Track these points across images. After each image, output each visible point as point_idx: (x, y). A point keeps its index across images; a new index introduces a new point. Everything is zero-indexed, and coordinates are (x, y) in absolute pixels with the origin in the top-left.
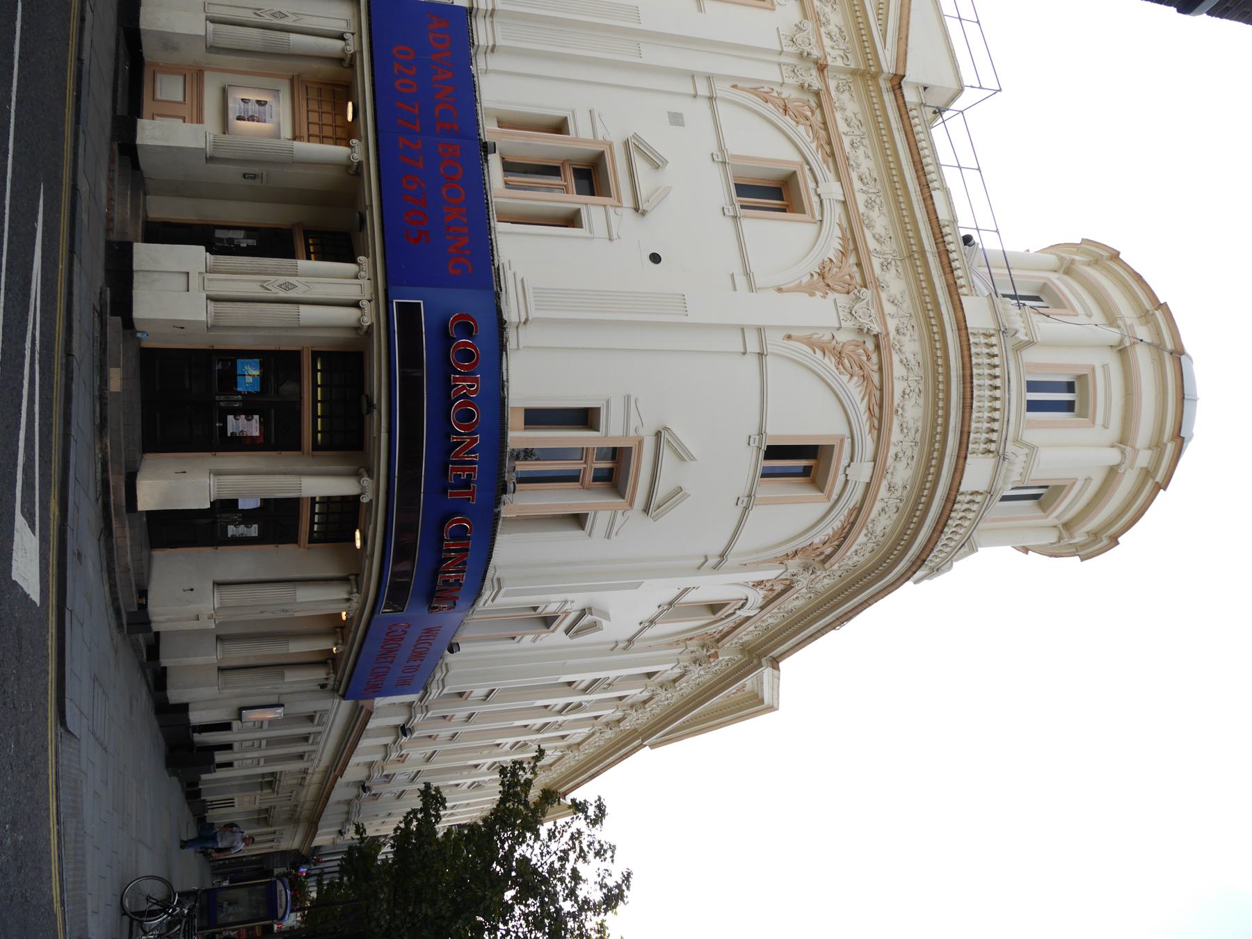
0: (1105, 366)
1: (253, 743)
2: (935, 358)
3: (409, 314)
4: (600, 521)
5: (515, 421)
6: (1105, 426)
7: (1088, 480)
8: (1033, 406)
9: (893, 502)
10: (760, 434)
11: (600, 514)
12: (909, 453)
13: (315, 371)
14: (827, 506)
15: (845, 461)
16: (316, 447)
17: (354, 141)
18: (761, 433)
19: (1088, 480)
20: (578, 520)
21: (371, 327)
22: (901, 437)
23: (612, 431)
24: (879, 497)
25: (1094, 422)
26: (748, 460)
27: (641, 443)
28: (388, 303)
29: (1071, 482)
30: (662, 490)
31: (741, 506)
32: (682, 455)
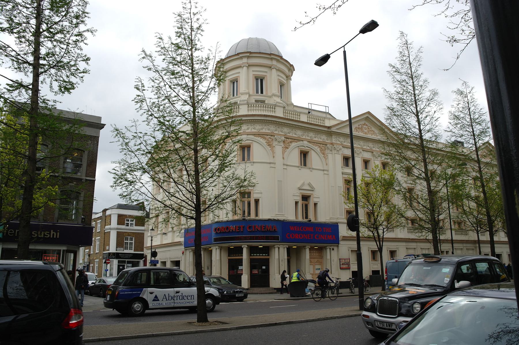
0: (253, 71)
1: (189, 284)
2: (265, 122)
3: (216, 240)
4: (316, 200)
5: (236, 218)
6: (266, 72)
7: (278, 75)
8: (262, 92)
9: (279, 129)
10: (299, 167)
11: (314, 200)
12: (294, 131)
13: (254, 256)
14: (312, 152)
15: (303, 147)
16: (269, 255)
17: (242, 247)
18: (298, 167)
19: (278, 75)
20: (315, 204)
21: (247, 245)
22: (304, 136)
23: (299, 199)
24: (291, 135)
25: (266, 75)
26: (305, 171)
27: (301, 193)
28: (214, 244)
29: (279, 80)
30: (309, 188)
31: (312, 170)
32: (303, 184)
